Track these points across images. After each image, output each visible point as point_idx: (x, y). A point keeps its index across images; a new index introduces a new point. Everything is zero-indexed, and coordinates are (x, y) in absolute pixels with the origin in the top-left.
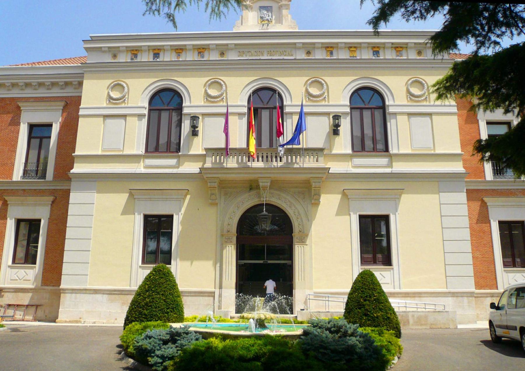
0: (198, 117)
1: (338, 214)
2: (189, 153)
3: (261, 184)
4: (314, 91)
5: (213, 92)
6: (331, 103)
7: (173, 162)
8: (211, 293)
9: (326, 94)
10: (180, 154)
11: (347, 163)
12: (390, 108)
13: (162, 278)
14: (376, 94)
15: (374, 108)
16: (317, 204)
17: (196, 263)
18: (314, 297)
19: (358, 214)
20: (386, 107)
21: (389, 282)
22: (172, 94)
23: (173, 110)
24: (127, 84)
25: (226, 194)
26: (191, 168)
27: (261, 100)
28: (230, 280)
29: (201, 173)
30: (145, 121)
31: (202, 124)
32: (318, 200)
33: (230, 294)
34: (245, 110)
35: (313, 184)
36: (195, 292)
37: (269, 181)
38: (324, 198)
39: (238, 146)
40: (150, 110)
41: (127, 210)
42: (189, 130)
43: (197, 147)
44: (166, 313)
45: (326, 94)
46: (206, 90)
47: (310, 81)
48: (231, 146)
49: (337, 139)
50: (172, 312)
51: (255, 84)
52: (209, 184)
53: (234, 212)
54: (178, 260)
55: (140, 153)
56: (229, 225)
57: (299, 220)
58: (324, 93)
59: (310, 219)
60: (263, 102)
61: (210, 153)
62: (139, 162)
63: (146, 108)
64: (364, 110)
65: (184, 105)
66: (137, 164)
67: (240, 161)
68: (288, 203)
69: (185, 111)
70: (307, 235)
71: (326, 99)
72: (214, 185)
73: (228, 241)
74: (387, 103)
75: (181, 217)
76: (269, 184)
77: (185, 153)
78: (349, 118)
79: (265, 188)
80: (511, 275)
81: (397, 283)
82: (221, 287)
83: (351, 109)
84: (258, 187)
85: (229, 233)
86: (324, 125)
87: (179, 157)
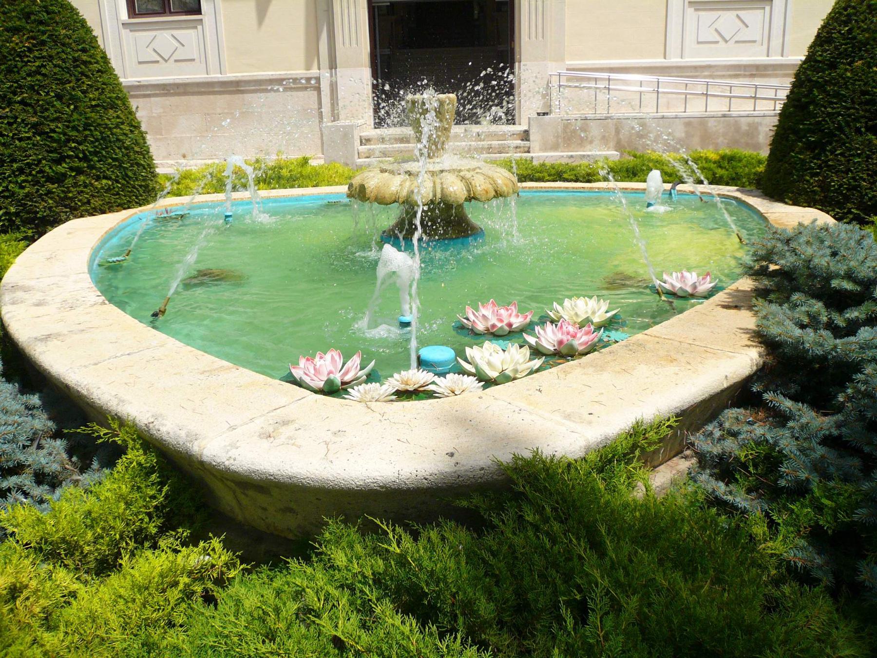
13: (16, 30)
18: (568, 80)
21: (758, 37)
28: (354, 42)
33: (357, 78)
44: (50, 180)
50: (79, 171)
81: (776, 43)
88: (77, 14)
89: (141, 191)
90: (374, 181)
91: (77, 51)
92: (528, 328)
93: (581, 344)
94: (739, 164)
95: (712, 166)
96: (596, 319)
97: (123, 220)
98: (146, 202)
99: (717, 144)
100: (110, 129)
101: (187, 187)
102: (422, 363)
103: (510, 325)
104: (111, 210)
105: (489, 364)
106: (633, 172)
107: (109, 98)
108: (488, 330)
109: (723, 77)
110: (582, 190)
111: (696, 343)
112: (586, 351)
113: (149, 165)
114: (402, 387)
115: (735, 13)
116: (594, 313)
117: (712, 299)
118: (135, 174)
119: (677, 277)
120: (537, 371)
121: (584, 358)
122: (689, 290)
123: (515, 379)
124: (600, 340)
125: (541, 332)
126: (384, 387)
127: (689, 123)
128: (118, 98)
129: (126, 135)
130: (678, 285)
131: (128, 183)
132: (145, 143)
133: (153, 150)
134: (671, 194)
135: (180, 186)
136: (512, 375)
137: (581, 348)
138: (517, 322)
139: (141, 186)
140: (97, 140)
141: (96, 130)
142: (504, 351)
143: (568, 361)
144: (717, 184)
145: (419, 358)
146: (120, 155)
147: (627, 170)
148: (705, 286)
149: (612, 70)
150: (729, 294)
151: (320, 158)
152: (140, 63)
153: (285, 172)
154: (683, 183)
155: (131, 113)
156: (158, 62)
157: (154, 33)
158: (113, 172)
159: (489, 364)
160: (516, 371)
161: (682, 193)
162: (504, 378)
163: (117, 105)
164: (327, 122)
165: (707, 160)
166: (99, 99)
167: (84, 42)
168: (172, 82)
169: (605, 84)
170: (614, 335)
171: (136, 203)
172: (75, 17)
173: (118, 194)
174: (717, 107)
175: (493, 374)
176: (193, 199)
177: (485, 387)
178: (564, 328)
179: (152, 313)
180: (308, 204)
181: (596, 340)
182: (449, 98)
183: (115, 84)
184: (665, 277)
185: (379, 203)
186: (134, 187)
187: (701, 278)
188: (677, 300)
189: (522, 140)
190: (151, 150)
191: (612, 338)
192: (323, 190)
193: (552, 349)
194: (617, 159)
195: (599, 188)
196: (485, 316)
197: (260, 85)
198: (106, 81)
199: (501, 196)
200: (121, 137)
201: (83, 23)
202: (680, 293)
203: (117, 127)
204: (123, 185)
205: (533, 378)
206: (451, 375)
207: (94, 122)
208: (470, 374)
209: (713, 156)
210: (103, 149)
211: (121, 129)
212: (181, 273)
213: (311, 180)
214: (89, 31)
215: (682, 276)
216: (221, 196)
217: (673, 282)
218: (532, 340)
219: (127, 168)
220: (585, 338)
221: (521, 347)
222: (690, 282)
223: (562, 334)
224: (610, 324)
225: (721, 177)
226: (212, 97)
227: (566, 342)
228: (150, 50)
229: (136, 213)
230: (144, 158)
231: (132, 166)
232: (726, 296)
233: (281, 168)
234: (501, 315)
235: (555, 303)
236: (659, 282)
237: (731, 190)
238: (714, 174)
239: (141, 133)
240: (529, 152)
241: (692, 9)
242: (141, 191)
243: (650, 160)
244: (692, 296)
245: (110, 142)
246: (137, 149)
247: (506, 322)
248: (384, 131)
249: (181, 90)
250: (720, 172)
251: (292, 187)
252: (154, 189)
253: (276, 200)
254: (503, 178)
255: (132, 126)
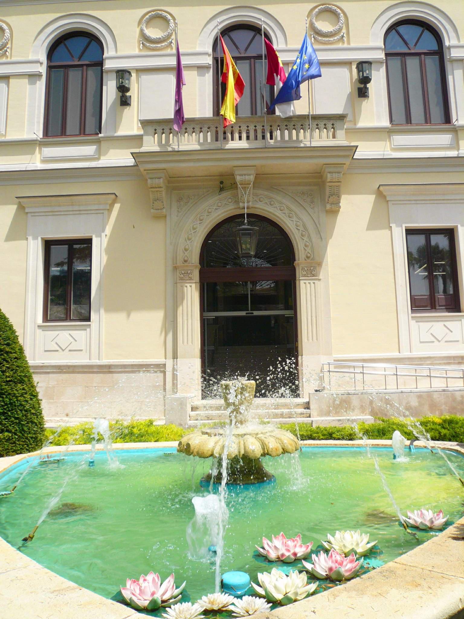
0: (129, 73)
1: (368, 229)
2: (116, 135)
3: (238, 178)
4: (324, 26)
5: (154, 33)
6: (353, 45)
7: (89, 150)
8: (157, 366)
9: (344, 31)
10: (100, 135)
11: (383, 143)
12: (452, 50)
14: (426, 31)
15: (425, 54)
16: (334, 211)
17: (136, 316)
18: (335, 368)
19: (404, 226)
20: (446, 52)
22: (86, 40)
23: (88, 65)
24: (8, 24)
25: (180, 200)
26: (120, 158)
27: (235, 44)
29: (137, 165)
30: (41, 85)
31: (136, 85)
32: (337, 203)
33: (191, 365)
34: (209, 60)
35: (329, 175)
36: (133, 366)
37: (253, 172)
38: (346, 202)
39: (197, 115)
40: (50, 68)
41: (16, 232)
42: (114, 97)
43: (129, 124)
45: (344, 31)
46: (142, 30)
47: (317, 10)
48: (187, 114)
49: (365, 104)
51: (225, 17)
52: (149, 181)
53: (194, 229)
54: (102, 311)
55: (34, 137)
56: (186, 250)
57: (305, 239)
58: (340, 30)
59: (323, 234)
60: (237, 47)
61: (151, 129)
62: (33, 153)
63: (41, 64)
64: (407, 58)
65: (105, 55)
66: (29, 157)
67: (201, 141)
68: (286, 211)
69: (108, 65)
70: (320, 264)
71: (345, 39)
72: (160, 184)
73: (185, 277)
74: (447, 43)
75: (105, 241)
76: (252, 178)
77: (109, 134)
78: (383, 70)
79: (245, 184)
80: (425, 326)
82: (175, 356)
83: (387, 55)
84: (234, 186)
85: (186, 264)
86: (341, 81)
87: (98, 142)
88: (8, 322)
89: (32, 442)
90: (196, 440)
91: (3, 345)
92: (307, 558)
93: (346, 571)
94: (457, 426)
95: (438, 427)
96: (360, 550)
97: (15, 463)
98: (34, 449)
99: (441, 410)
100: (17, 397)
101: (65, 439)
102: (225, 587)
103: (295, 554)
104: (7, 455)
105: (275, 587)
106: (382, 433)
107: (20, 376)
108: (278, 558)
109: (440, 364)
110: (347, 446)
111: (434, 570)
112: (350, 577)
113: (40, 423)
114: (209, 607)
115: (442, 323)
116: (358, 544)
117: (444, 532)
118: (29, 429)
119: (418, 514)
120: (313, 594)
121: (349, 583)
122: (428, 524)
123: (296, 601)
124: (362, 567)
125: (316, 558)
126: (196, 606)
127: (420, 396)
128: (25, 376)
129: (27, 401)
130: (419, 520)
131: (23, 435)
132: (40, 407)
133: (44, 413)
134: (410, 448)
135: (60, 438)
136: (293, 597)
137: (347, 574)
138: (301, 551)
139: (32, 438)
140: (6, 404)
141: (7, 397)
142: (287, 576)
143: (337, 585)
144: (443, 440)
145: (222, 581)
146: (20, 416)
147: (378, 431)
148: (440, 521)
149: (365, 361)
150: (457, 528)
151: (163, 419)
152: (46, 351)
153: (135, 430)
154: (418, 440)
155: (33, 386)
156: (57, 351)
157: (57, 333)
158: (13, 427)
159: (275, 587)
160: (296, 594)
161: (417, 447)
162: (287, 601)
163: (24, 381)
164: (170, 395)
165: (434, 423)
166: (12, 377)
167: (9, 339)
168: (65, 364)
169: (360, 370)
170: (373, 562)
171: (27, 450)
172: (6, 323)
173: (14, 443)
174: (438, 384)
175: (279, 596)
176: (68, 448)
177: (272, 608)
178: (334, 556)
179: (23, 538)
180: (152, 455)
181: (358, 568)
182: (251, 384)
183: (25, 367)
184: (409, 514)
185: (200, 457)
186: (27, 438)
187: (436, 514)
188: (428, 529)
189: (305, 408)
190: (43, 412)
191: (371, 566)
192: (162, 444)
193: (324, 574)
194: (372, 422)
195: (358, 445)
196: (275, 547)
197: (125, 368)
198: (19, 365)
199: (287, 452)
200: (23, 403)
201: (11, 327)
202: (421, 527)
203: (22, 395)
204: (19, 436)
205: (309, 601)
206: (247, 596)
207: (6, 392)
208: (260, 596)
209: (437, 420)
210: (9, 411)
211: (24, 397)
212: (53, 503)
213: (154, 437)
214: (14, 332)
215: (422, 514)
216: (88, 447)
217: (415, 518)
218: (309, 566)
219: (24, 425)
220: (349, 566)
221: (300, 572)
222: (428, 518)
223: (332, 562)
224: (370, 554)
225: (445, 435)
226: (91, 375)
227: (335, 569)
228: (53, 343)
229: (25, 457)
230: (37, 417)
231: (28, 423)
232: (455, 530)
233: (133, 427)
234: (288, 546)
235: (329, 535)
236: (404, 518)
237: (453, 445)
238: (440, 433)
239: (38, 400)
240: (310, 417)
241: (415, 321)
242: (32, 442)
243: (394, 424)
244: (431, 529)
245: (15, 406)
246: (33, 411)
247: (292, 551)
248: (209, 402)
249: (71, 370)
250: (444, 431)
251: (140, 441)
252: (41, 440)
253: (128, 451)
254: (288, 438)
255: (32, 395)
